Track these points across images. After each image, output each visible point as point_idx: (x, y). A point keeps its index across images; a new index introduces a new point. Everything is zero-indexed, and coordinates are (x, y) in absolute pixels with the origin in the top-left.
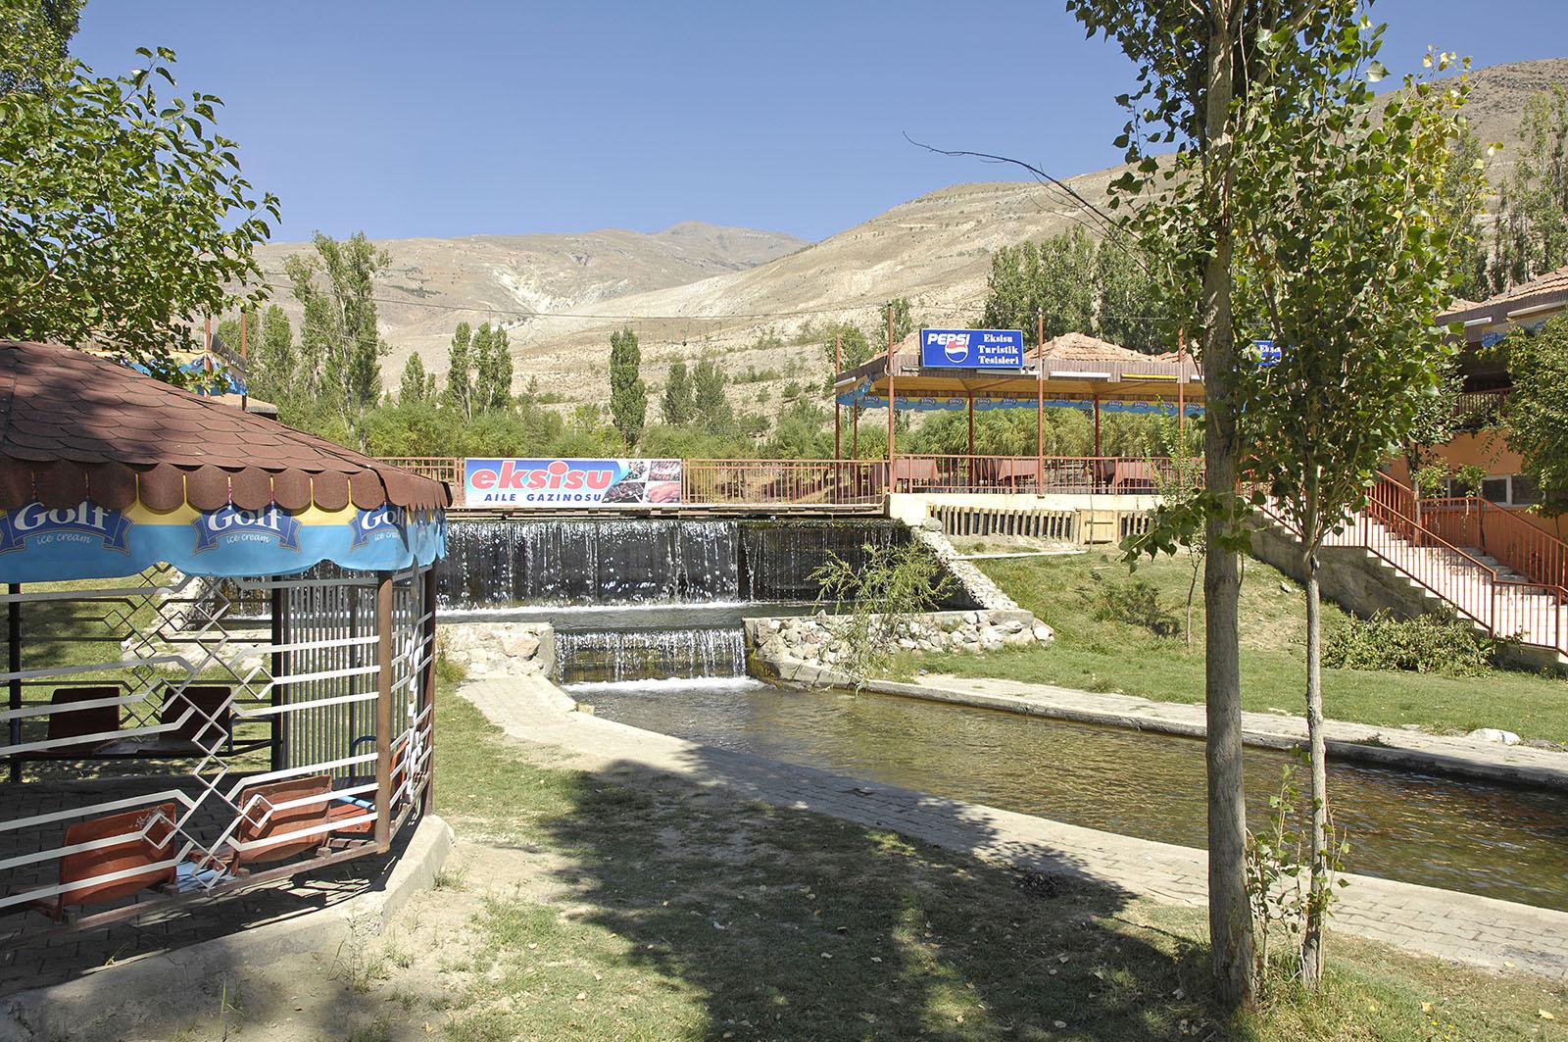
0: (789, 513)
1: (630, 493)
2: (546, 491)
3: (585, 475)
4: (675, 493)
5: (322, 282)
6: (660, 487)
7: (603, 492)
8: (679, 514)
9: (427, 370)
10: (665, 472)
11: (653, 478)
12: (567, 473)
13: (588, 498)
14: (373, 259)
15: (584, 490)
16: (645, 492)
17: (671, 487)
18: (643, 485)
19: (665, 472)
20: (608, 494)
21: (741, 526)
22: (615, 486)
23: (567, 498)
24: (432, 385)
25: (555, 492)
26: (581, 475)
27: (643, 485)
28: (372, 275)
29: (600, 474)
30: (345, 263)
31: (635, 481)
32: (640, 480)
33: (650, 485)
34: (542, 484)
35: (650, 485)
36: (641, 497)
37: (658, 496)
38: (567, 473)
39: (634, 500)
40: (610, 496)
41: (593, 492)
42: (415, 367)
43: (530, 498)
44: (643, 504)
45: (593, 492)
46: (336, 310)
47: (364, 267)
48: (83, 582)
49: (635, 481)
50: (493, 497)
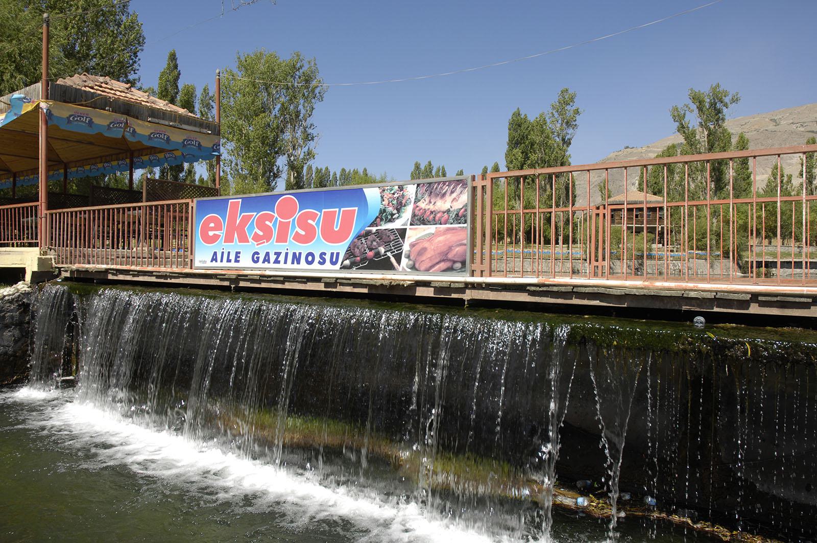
0: (754, 309)
1: (382, 250)
2: (272, 246)
3: (318, 217)
4: (458, 249)
5: (693, 120)
6: (431, 237)
7: (341, 248)
8: (468, 295)
9: (787, 172)
10: (442, 205)
11: (419, 219)
12: (297, 215)
13: (296, 258)
14: (727, 100)
15: (319, 246)
16: (406, 248)
17: (451, 238)
18: (402, 233)
19: (442, 205)
20: (350, 253)
21: (577, 340)
22: (359, 237)
23: (296, 258)
24: (789, 180)
25: (282, 248)
26: (313, 217)
27: (402, 233)
28: (725, 110)
29: (339, 212)
30: (707, 105)
31: (390, 226)
32: (397, 225)
33: (414, 234)
34: (267, 236)
35: (414, 234)
36: (398, 258)
37: (428, 254)
38: (297, 215)
39: (386, 265)
40: (355, 258)
41: (330, 248)
42: (205, 90)
43: (255, 258)
44: (402, 274)
45: (330, 248)
46: (702, 136)
47: (719, 105)
48: (764, 300)
49: (390, 226)
50: (273, 258)
